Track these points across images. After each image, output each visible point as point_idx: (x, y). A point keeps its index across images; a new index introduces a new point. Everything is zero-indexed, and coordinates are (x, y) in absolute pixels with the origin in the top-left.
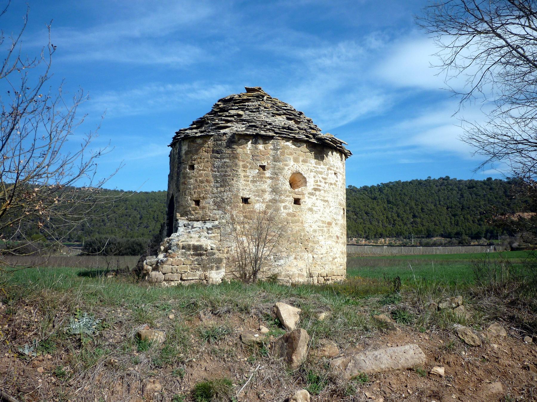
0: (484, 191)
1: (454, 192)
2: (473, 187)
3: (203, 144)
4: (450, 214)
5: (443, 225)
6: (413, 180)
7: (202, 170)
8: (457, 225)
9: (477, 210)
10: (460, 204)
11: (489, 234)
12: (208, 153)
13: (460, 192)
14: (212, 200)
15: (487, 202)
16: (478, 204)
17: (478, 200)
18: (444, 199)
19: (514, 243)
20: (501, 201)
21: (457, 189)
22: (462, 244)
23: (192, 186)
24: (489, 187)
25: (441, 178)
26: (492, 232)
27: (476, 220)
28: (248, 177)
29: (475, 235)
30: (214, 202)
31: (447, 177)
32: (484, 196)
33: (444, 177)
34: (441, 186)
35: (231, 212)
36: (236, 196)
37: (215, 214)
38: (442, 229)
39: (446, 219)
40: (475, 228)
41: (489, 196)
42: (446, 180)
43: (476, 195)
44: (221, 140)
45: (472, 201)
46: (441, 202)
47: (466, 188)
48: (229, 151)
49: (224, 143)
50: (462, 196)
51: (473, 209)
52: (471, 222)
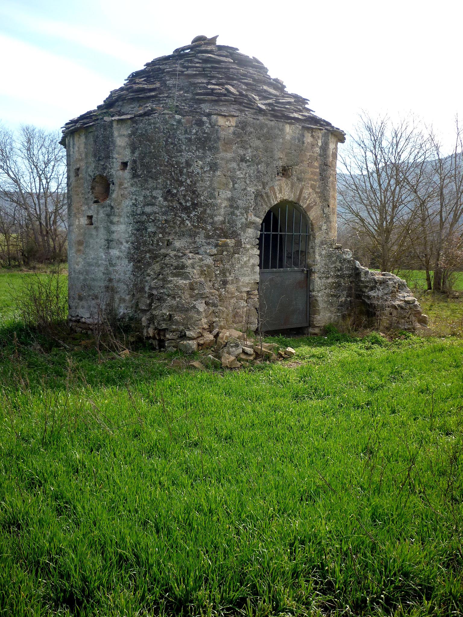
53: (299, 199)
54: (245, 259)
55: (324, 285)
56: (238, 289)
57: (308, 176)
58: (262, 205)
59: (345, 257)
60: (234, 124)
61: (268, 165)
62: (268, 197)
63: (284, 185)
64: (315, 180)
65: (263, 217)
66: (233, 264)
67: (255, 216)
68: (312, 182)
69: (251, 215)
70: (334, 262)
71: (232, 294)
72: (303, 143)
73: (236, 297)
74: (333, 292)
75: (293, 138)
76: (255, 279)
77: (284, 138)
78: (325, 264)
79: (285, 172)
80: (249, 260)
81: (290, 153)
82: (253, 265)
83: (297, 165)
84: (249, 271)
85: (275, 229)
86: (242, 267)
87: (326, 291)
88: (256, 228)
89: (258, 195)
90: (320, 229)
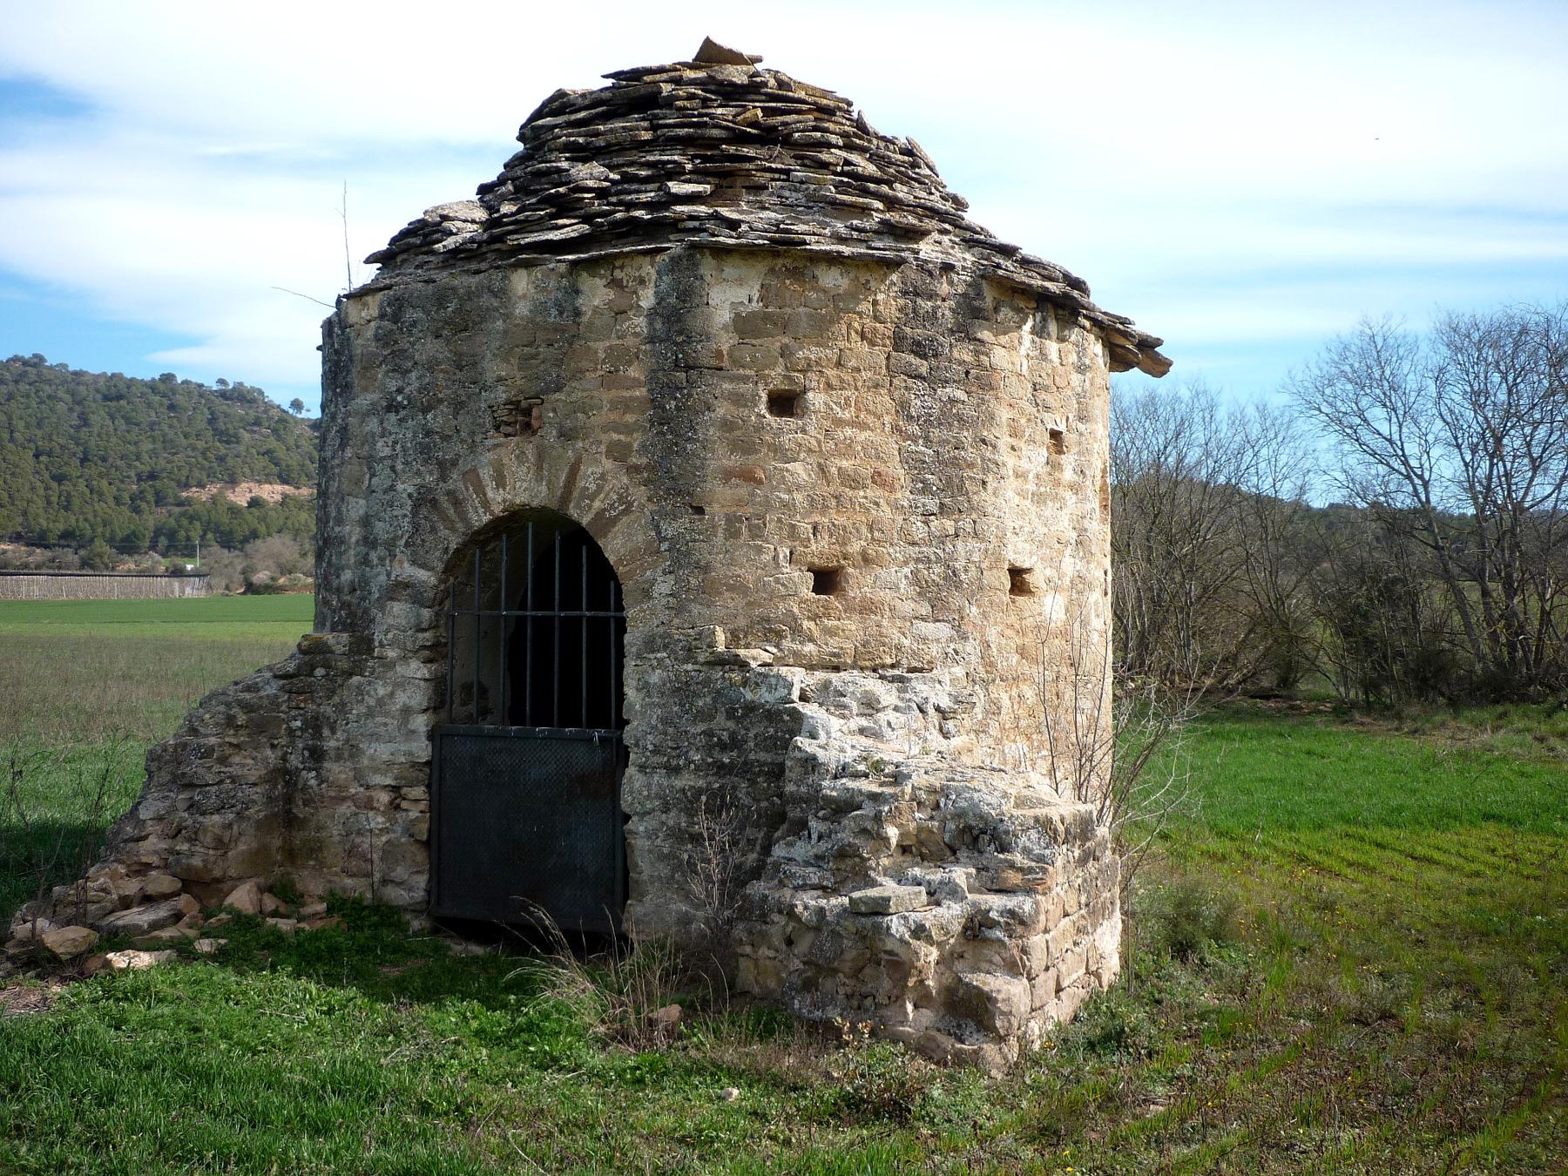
0: (153, 414)
1: (61, 407)
2: (119, 397)
3: (853, 296)
4: (47, 475)
5: (21, 505)
7: (852, 424)
8: (67, 508)
9: (129, 466)
10: (77, 444)
11: (163, 541)
12: (872, 344)
13: (78, 408)
14: (907, 570)
15: (159, 445)
16: (132, 448)
17: (132, 437)
18: (27, 426)
19: (254, 571)
20: (201, 445)
21: (68, 398)
22: (92, 567)
23: (799, 497)
24: (166, 402)
25: (16, 359)
26: (172, 535)
27: (126, 496)
29: (122, 540)
30: (916, 579)
31: (35, 356)
32: (152, 426)
33: (27, 355)
34: (16, 382)
37: (925, 639)
38: (20, 519)
39: (33, 489)
40: (123, 521)
41: (166, 427)
42: (35, 365)
43: (128, 421)
44: (931, 296)
45: (113, 439)
46: (17, 435)
47: (99, 396)
48: (964, 353)
49: (946, 311)
50: (84, 421)
51: (119, 463)
52: (112, 502)
53: (565, 498)
54: (381, 692)
55: (658, 796)
56: (358, 777)
58: (434, 530)
59: (749, 696)
60: (375, 312)
61: (458, 406)
62: (457, 503)
63: (509, 460)
64: (628, 429)
65: (440, 566)
66: (344, 704)
67: (413, 563)
68: (615, 436)
69: (401, 562)
70: (706, 716)
71: (342, 788)
72: (577, 313)
73: (352, 798)
75: (540, 308)
76: (411, 754)
77: (507, 317)
78: (664, 721)
79: (521, 418)
80: (392, 694)
81: (534, 357)
82: (407, 711)
83: (559, 389)
84: (390, 728)
85: (571, 601)
86: (370, 714)
87: (671, 819)
88: (418, 601)
89: (424, 500)
90: (647, 594)
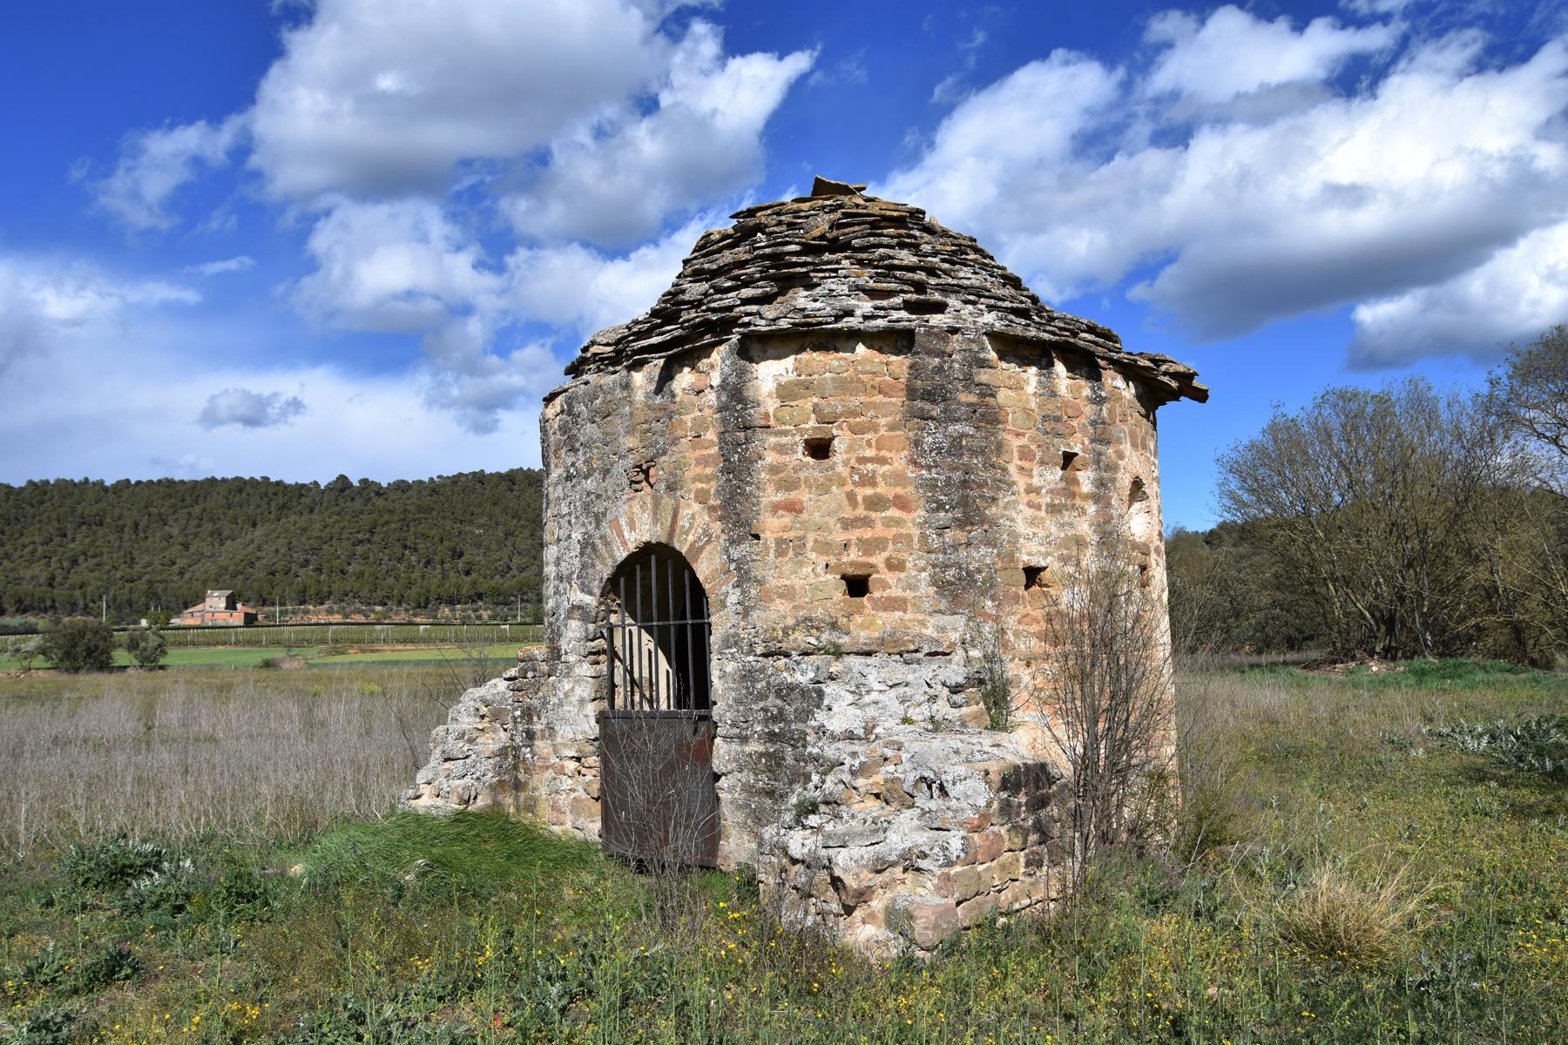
6: (461, 474)
28: (1037, 491)
35: (997, 619)
36: (1011, 557)
55: (736, 760)
57: (693, 471)
62: (607, 544)
68: (700, 485)
74: (763, 781)
78: (738, 701)
83: (664, 453)
89: (587, 544)
90: (723, 605)
